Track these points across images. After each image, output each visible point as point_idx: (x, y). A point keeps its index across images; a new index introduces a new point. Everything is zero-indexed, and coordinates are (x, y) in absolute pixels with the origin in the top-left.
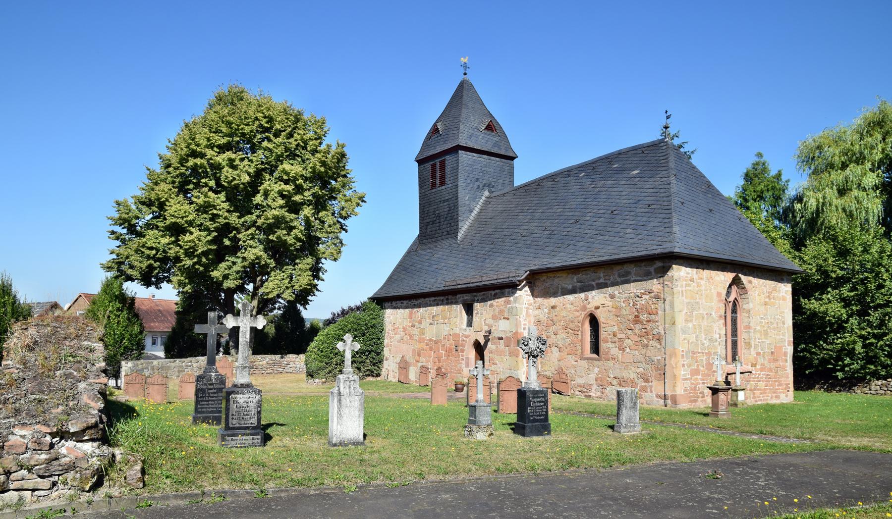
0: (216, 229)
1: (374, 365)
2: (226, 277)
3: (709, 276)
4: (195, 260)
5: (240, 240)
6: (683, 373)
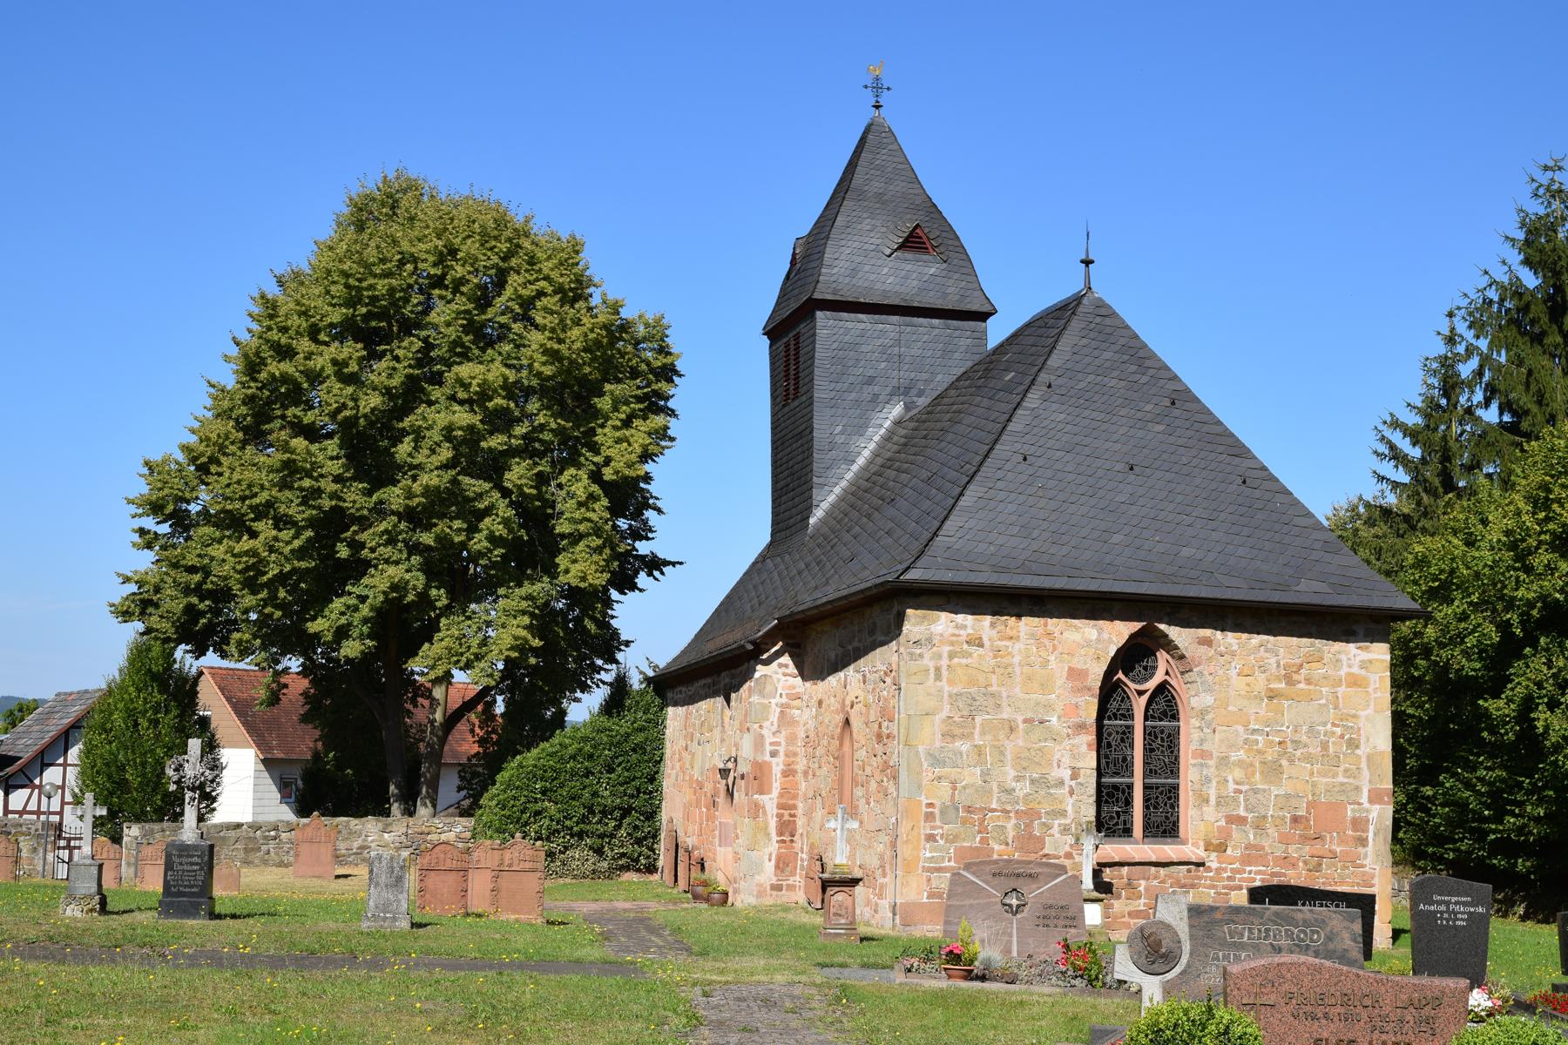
0: (312, 523)
1: (639, 842)
2: (342, 633)
3: (1041, 630)
4: (264, 594)
5: (362, 545)
6: (928, 855)
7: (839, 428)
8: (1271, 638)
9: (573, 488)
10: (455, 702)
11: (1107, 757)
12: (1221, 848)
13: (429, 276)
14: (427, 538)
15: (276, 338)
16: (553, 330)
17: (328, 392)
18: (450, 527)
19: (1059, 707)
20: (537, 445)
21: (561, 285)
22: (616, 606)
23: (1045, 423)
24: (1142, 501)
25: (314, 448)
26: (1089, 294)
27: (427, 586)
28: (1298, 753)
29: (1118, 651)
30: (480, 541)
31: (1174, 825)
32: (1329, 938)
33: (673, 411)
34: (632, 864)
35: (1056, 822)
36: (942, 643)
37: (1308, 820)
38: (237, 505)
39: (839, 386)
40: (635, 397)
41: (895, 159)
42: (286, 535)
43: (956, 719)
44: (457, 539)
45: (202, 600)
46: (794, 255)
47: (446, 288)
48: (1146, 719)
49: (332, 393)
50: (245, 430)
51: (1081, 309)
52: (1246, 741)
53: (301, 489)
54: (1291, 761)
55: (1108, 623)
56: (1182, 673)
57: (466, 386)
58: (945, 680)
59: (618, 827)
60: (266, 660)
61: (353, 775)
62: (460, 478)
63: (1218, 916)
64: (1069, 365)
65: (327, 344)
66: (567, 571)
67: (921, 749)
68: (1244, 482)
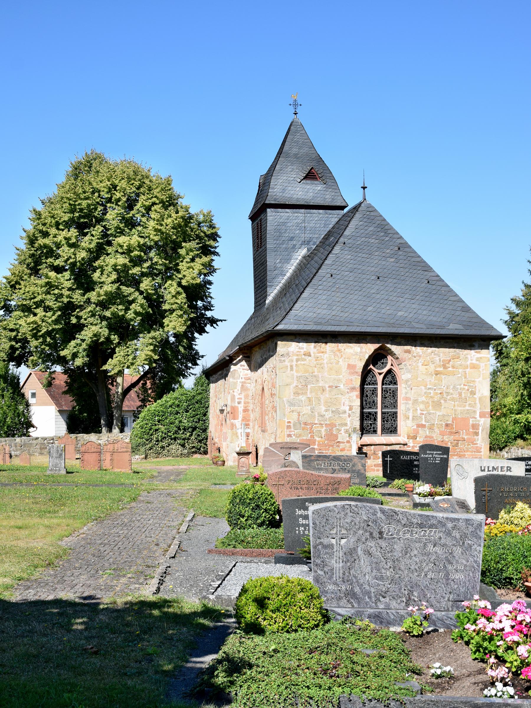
0: (60, 309)
1: (200, 441)
2: (75, 356)
3: (336, 349)
4: (41, 340)
7: (278, 261)
8: (437, 349)
9: (170, 290)
10: (126, 385)
11: (366, 401)
12: (415, 438)
13: (106, 198)
14: (108, 314)
15: (41, 228)
16: (158, 220)
17: (63, 252)
18: (117, 309)
19: (344, 381)
20: (155, 271)
21: (162, 200)
22: (197, 340)
23: (342, 260)
24: (382, 292)
25: (59, 276)
26: (365, 202)
27: (109, 335)
28: (448, 397)
29: (370, 356)
30: (131, 314)
31: (395, 428)
32: (353, 466)
33: (217, 253)
34: (197, 451)
35: (343, 428)
36: (293, 355)
37: (452, 425)
38: (28, 302)
39: (278, 242)
40: (195, 248)
41: (303, 138)
42: (49, 314)
43: (299, 387)
44: (120, 314)
45: (17, 343)
46: (260, 183)
47: (113, 203)
48: (383, 384)
49: (65, 252)
50: (31, 269)
51: (360, 209)
52: (425, 393)
53: (55, 294)
54: (445, 401)
55: (365, 345)
56: (398, 365)
57: (121, 246)
58: (294, 371)
59: (191, 435)
60: (44, 368)
61: (87, 416)
62: (121, 287)
63: (313, 458)
64: (354, 234)
65: (63, 230)
66: (168, 326)
67: (285, 399)
68: (428, 282)
